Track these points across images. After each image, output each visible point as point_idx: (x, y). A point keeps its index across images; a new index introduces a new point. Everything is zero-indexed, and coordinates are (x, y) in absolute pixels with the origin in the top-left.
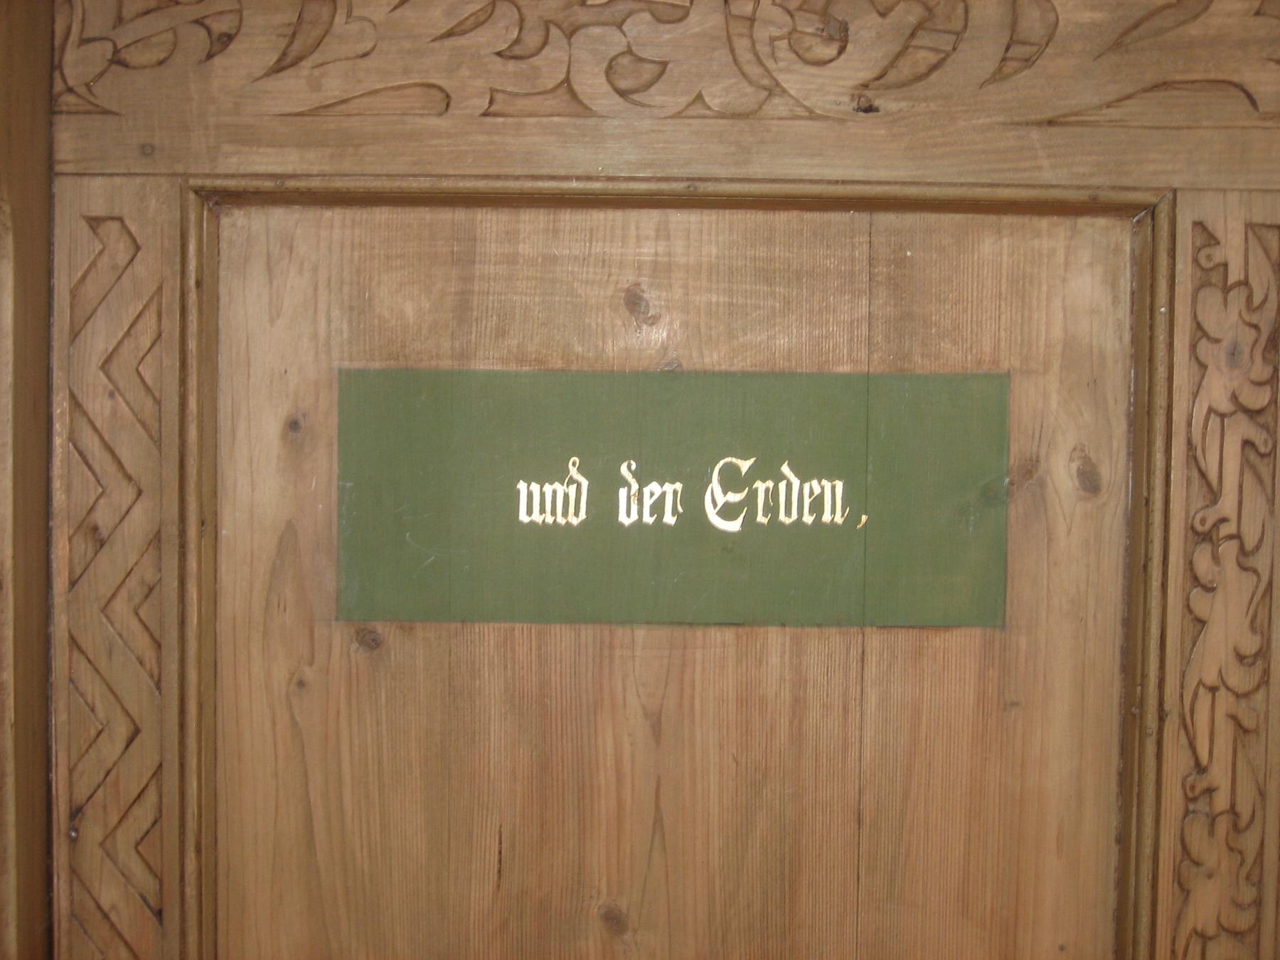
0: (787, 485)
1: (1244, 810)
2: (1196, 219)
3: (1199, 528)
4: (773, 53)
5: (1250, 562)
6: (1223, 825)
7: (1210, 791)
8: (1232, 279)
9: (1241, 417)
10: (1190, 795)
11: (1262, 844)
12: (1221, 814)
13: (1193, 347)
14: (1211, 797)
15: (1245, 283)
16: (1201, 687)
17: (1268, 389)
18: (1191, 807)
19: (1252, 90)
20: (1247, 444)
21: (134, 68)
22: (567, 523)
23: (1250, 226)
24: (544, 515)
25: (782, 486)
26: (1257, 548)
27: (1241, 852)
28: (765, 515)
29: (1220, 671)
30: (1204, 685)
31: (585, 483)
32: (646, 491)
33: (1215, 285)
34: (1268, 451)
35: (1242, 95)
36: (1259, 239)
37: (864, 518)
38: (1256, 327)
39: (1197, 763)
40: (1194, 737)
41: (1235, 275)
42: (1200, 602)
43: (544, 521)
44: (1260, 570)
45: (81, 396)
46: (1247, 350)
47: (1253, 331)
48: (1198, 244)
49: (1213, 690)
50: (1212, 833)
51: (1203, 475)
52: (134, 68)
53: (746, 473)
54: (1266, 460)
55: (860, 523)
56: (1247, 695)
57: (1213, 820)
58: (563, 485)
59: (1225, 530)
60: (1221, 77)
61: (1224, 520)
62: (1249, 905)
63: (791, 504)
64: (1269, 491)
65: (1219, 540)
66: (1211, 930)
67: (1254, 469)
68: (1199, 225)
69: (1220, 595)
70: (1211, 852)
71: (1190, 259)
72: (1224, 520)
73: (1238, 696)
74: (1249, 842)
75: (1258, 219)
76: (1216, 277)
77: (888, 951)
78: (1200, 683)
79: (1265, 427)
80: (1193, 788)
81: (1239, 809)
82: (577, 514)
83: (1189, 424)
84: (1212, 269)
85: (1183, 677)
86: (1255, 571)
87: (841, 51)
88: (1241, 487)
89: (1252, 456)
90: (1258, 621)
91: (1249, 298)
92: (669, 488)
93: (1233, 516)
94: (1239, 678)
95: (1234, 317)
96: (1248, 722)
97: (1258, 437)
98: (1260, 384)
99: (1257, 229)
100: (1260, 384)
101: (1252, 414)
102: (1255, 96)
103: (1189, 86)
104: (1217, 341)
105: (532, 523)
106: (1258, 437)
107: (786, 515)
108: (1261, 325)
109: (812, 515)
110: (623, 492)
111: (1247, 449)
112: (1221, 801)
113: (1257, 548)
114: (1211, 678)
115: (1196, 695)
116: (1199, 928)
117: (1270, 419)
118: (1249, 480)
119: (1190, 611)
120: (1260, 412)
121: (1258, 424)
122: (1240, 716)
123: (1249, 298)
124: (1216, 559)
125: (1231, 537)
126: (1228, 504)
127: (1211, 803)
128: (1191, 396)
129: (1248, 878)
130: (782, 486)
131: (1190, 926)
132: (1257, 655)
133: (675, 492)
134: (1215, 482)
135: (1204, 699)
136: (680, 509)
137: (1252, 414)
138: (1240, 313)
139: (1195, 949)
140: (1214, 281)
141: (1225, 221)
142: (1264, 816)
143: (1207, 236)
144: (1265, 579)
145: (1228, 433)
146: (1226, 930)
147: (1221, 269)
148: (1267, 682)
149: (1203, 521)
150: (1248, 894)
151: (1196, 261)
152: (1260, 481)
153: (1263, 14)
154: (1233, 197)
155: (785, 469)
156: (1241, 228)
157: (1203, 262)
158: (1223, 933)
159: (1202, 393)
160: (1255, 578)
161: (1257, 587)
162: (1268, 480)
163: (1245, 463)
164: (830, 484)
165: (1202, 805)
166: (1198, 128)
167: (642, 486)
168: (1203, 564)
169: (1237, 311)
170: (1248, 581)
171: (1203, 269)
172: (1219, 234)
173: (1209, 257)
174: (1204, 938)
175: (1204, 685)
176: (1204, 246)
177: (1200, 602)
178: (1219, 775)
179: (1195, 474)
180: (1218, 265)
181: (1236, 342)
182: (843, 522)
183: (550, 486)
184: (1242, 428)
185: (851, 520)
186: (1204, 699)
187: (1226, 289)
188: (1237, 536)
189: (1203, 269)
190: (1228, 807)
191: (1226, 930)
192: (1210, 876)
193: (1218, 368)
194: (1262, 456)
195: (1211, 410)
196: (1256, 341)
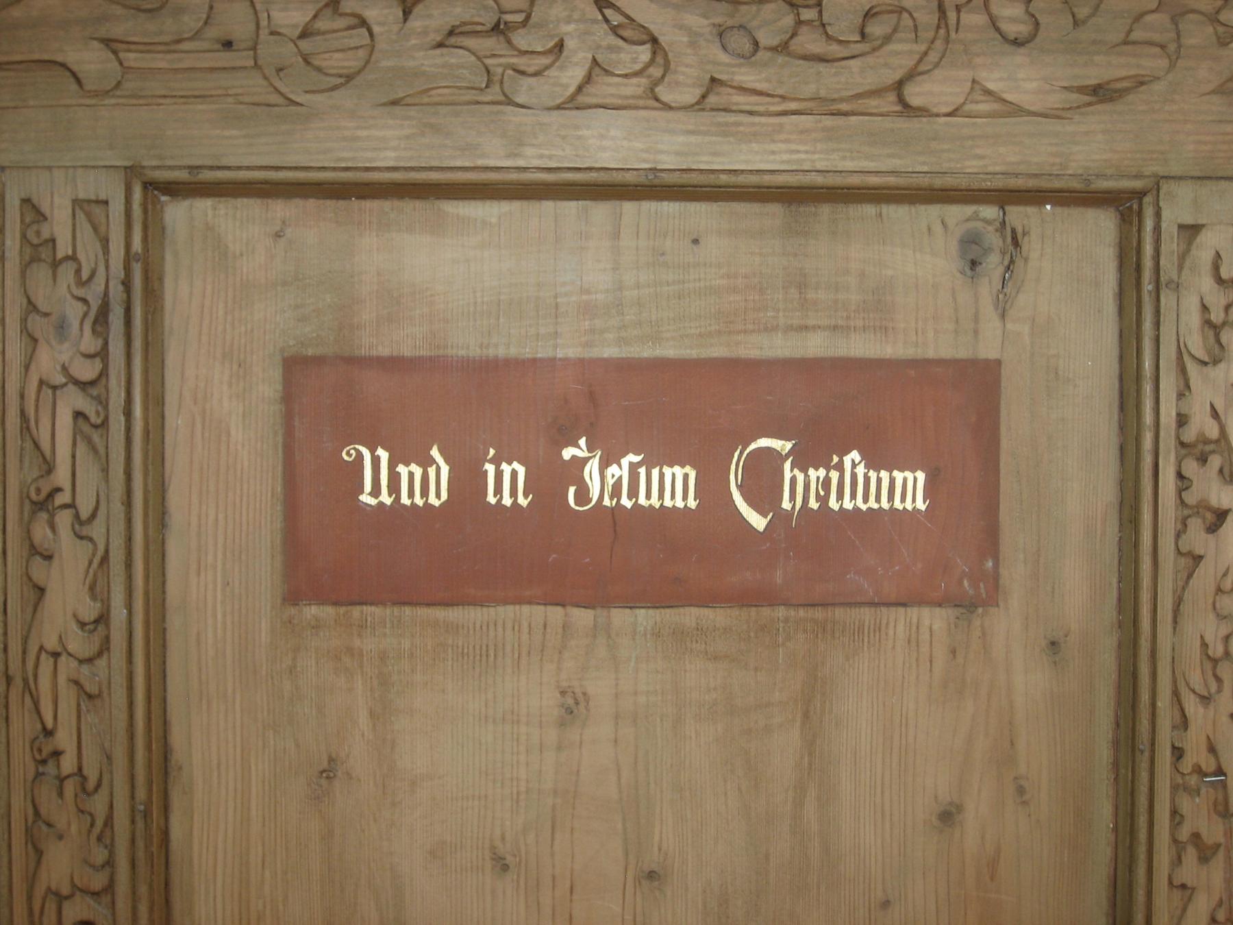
0: (437, 469)
1: (92, 775)
2: (23, 196)
3: (34, 496)
5: (85, 531)
6: (70, 788)
7: (57, 754)
8: (60, 255)
9: (71, 388)
10: (38, 757)
11: (111, 807)
12: (68, 777)
13: (24, 321)
14: (58, 761)
15: (73, 258)
16: (43, 653)
17: (98, 361)
18: (41, 769)
19: (75, 68)
20: (78, 415)
23: (76, 202)
26: (94, 516)
27: (91, 814)
29: (60, 637)
30: (46, 651)
31: (445, 470)
33: (44, 261)
34: (99, 421)
35: (68, 74)
36: (88, 215)
38: (84, 301)
39: (44, 728)
40: (38, 701)
41: (63, 249)
42: (38, 570)
44: (95, 537)
46: (75, 324)
47: (80, 304)
48: (28, 220)
49: (56, 655)
50: (61, 794)
51: (37, 445)
54: (100, 431)
56: (90, 660)
57: (62, 780)
59: (61, 499)
60: (46, 57)
61: (59, 490)
62: (103, 866)
64: (104, 459)
65: (54, 509)
66: (65, 891)
67: (89, 441)
68: (26, 201)
69: (56, 562)
70: (61, 813)
71: (18, 235)
72: (59, 490)
73: (81, 662)
74: (98, 805)
75: (82, 196)
76: (45, 253)
78: (41, 648)
79: (98, 399)
80: (40, 750)
81: (85, 772)
83: (22, 396)
84: (41, 245)
85: (26, 642)
86: (91, 540)
87: (1172, 66)
88: (74, 457)
89: (86, 428)
90: (98, 589)
91: (78, 271)
93: (67, 486)
94: (78, 644)
95: (62, 289)
96: (91, 688)
97: (89, 408)
98: (90, 356)
99: (85, 206)
100: (90, 356)
101: (83, 385)
102: (80, 75)
103: (15, 66)
104: (46, 315)
105: (870, 509)
106: (89, 408)
108: (89, 298)
111: (81, 421)
112: (68, 764)
113: (94, 516)
114: (51, 643)
115: (38, 658)
116: (53, 887)
117: (103, 390)
118: (82, 449)
119: (30, 579)
120: (93, 383)
121: (92, 397)
122: (83, 681)
123: (78, 271)
124: (53, 527)
125: (66, 506)
126: (62, 476)
127: (58, 766)
128: (23, 369)
129: (99, 839)
130: (432, 471)
131: (44, 887)
132: (96, 622)
133: (818, 478)
134: (48, 453)
135: (46, 663)
137: (83, 385)
138: (69, 286)
139: (51, 907)
140: (43, 256)
141: (52, 197)
142: (112, 781)
143: (33, 211)
144: (101, 548)
145: (59, 403)
146: (81, 890)
147: (51, 244)
148: (108, 649)
149: (38, 491)
150: (100, 855)
151: (24, 236)
152: (95, 450)
155: (435, 452)
156: (69, 204)
157: (31, 234)
158: (78, 893)
159: (33, 367)
160: (90, 545)
161: (94, 555)
162: (102, 451)
163: (76, 432)
164: (875, 474)
165: (50, 768)
166: (24, 107)
168: (41, 532)
169: (65, 286)
170: (85, 548)
171: (32, 245)
172: (45, 208)
173: (38, 233)
174: (61, 898)
175: (46, 651)
176: (33, 222)
177: (38, 570)
178: (64, 739)
179: (29, 445)
180: (46, 241)
181: (65, 316)
183: (670, 469)
184: (73, 400)
186: (46, 663)
187: (55, 264)
188: (71, 506)
189: (32, 245)
190: (76, 770)
191: (81, 890)
192: (61, 837)
193: (48, 342)
194: (96, 427)
195: (42, 383)
196: (85, 315)
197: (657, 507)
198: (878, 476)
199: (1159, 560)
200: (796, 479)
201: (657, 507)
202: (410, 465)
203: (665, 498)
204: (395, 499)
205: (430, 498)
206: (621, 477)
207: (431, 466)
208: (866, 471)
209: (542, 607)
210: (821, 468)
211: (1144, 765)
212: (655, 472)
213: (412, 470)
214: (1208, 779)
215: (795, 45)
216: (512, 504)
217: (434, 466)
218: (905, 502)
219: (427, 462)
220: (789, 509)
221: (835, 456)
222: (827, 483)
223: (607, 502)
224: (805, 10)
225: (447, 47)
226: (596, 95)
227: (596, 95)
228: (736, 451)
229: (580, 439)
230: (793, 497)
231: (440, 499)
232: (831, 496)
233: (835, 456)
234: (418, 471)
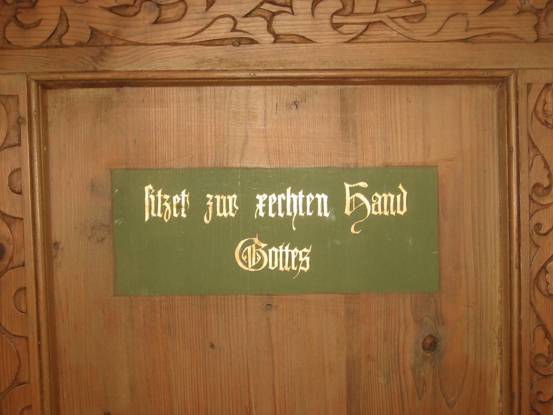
22: (383, 214)
24: (228, 213)
25: (399, 197)
28: (311, 211)
31: (405, 193)
32: (308, 197)
45: (535, 119)
55: (367, 216)
63: (226, 207)
82: (402, 209)
92: (230, 198)
130: (399, 197)
133: (233, 199)
136: (237, 208)
153: (537, 9)
155: (400, 187)
182: (235, 216)
183: (261, 196)
198: (226, 198)
199: (34, 263)
203: (324, 212)
204: (276, 214)
206: (181, 201)
207: (398, 194)
208: (162, 196)
213: (292, 197)
217: (400, 195)
220: (349, 214)
222: (315, 201)
225: (543, 89)
226: (215, 12)
227: (215, 12)
230: (292, 210)
231: (167, 219)
232: (392, 207)
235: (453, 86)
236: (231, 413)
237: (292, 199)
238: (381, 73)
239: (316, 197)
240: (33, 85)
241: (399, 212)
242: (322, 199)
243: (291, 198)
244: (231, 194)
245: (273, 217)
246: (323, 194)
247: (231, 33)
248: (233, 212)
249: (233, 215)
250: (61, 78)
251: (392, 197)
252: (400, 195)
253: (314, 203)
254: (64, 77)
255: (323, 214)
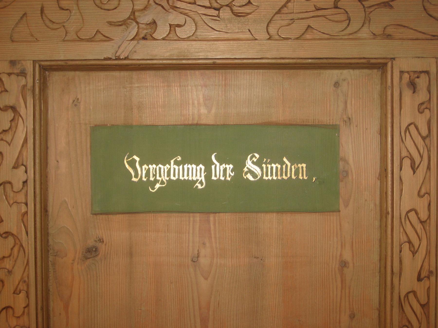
4: (18, 203)
21: (430, 286)
25: (284, 166)
37: (314, 179)
43: (188, 179)
52: (430, 286)
53: (181, 165)
58: (250, 161)
77: (298, 223)
92: (227, 166)
105: (185, 180)
107: (266, 177)
109: (168, 177)
110: (213, 167)
130: (284, 166)
154: (13, 77)
155: (285, 160)
167: (221, 165)
185: (310, 178)
197: (271, 179)
200: (145, 176)
201: (271, 179)
202: (192, 164)
205: (278, 177)
209: (198, 217)
210: (262, 166)
211: (389, 93)
212: (181, 167)
213: (193, 167)
214: (42, 109)
215: (9, 141)
216: (169, 179)
217: (215, 165)
218: (189, 176)
219: (282, 163)
220: (294, 178)
221: (265, 159)
223: (293, 177)
224: (8, 141)
228: (129, 161)
229: (259, 157)
233: (265, 159)
234: (279, 166)
235: (366, 70)
236: (137, 327)
237: (175, 169)
238: (299, 61)
239: (149, 167)
240: (37, 66)
241: (284, 177)
242: (193, 168)
243: (192, 167)
244: (229, 164)
245: (294, 178)
246: (154, 165)
247: (28, 77)
248: (229, 177)
249: (229, 179)
250: (38, 81)
251: (279, 166)
252: (215, 165)
253: (148, 171)
254: (37, 80)
255: (266, 166)
